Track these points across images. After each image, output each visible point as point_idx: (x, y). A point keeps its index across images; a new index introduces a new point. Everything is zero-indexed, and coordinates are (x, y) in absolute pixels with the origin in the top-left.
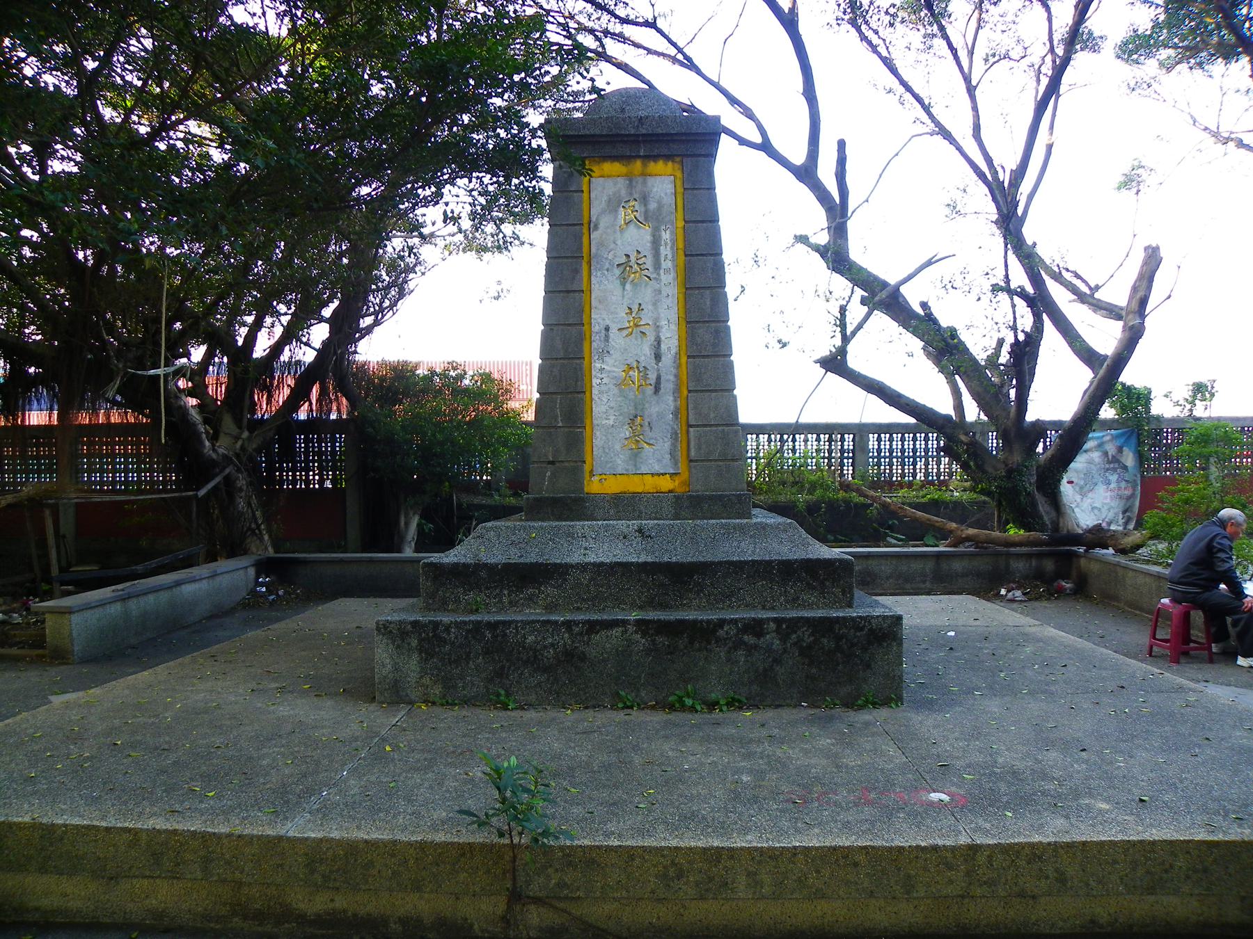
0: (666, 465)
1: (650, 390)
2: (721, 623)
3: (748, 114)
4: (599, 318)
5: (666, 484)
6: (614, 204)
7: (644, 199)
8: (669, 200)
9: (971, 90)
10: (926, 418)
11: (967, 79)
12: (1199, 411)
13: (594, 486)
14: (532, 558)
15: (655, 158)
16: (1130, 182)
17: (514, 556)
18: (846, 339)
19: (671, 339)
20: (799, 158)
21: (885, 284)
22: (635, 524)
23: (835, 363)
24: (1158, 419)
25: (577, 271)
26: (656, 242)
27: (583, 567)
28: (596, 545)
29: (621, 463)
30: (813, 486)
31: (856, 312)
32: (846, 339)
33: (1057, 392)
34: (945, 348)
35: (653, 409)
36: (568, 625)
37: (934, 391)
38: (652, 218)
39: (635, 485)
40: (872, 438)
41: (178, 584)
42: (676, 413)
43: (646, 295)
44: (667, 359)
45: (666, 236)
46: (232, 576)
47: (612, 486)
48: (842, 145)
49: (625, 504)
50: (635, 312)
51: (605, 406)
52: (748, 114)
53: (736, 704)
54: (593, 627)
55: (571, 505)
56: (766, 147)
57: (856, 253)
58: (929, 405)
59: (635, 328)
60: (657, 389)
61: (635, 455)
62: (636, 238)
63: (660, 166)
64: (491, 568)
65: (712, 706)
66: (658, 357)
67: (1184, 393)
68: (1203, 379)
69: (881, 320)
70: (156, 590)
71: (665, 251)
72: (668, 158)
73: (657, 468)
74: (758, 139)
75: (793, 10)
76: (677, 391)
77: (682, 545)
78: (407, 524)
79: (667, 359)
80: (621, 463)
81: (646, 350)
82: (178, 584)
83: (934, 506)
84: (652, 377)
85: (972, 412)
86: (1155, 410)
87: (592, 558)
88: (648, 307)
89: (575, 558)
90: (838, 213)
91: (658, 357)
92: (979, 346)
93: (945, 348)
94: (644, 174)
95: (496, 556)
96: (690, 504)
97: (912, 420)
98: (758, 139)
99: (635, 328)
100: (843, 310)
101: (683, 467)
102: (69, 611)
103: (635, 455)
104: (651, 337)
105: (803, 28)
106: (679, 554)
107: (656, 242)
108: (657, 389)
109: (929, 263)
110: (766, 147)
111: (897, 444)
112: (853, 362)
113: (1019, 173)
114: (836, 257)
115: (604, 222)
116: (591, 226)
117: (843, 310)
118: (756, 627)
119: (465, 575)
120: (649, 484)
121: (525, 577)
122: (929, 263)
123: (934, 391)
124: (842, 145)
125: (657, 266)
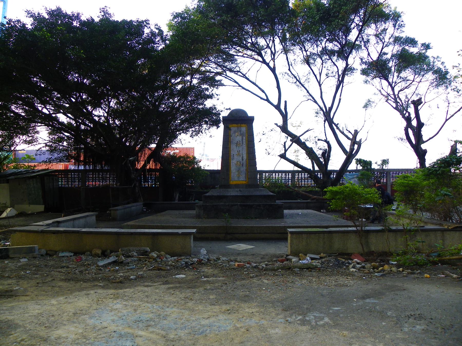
0: (244, 179)
1: (241, 166)
2: (254, 205)
3: (263, 91)
4: (232, 153)
5: (244, 182)
6: (235, 132)
7: (240, 131)
8: (245, 131)
9: (320, 85)
10: (304, 170)
11: (319, 83)
12: (384, 167)
13: (231, 183)
14: (222, 194)
15: (242, 124)
16: (366, 106)
17: (218, 194)
18: (286, 150)
19: (245, 157)
20: (276, 103)
21: (297, 136)
22: (239, 189)
23: (283, 156)
24: (374, 169)
25: (228, 144)
26: (242, 139)
27: (230, 196)
28: (232, 193)
29: (236, 179)
30: (280, 187)
31: (289, 143)
32: (286, 150)
33: (335, 163)
34: (310, 153)
35: (242, 169)
36: (228, 205)
37: (307, 163)
38: (242, 135)
39: (239, 183)
40: (274, 174)
41: (132, 206)
42: (246, 170)
43: (241, 149)
44: (244, 160)
45: (244, 138)
46: (136, 207)
47: (235, 183)
48: (286, 102)
49: (237, 186)
50: (239, 152)
51: (233, 168)
52: (263, 91)
53: (256, 218)
54: (232, 205)
55: (227, 186)
56: (267, 100)
57: (290, 128)
58: (306, 167)
59: (239, 155)
60: (243, 165)
61: (239, 177)
62: (239, 138)
63: (243, 125)
64: (215, 196)
65: (252, 218)
66: (243, 160)
67: (380, 163)
68: (385, 159)
69: (295, 146)
70: (128, 207)
71: (244, 141)
72: (245, 123)
73: (243, 180)
74: (265, 98)
75: (274, 67)
76: (246, 166)
77: (246, 193)
78: (176, 196)
79: (244, 160)
80: (236, 179)
81: (241, 158)
82: (132, 206)
83: (311, 192)
84: (242, 163)
85: (317, 168)
86: (373, 167)
87: (232, 194)
88: (241, 151)
89: (229, 195)
90: (285, 117)
91: (243, 160)
92: (319, 153)
93: (310, 153)
94: (240, 127)
95: (215, 194)
96: (248, 186)
97: (300, 170)
98: (265, 98)
99: (239, 155)
100: (285, 143)
101: (247, 179)
102: (117, 210)
103: (239, 177)
104: (241, 156)
105: (277, 72)
106: (246, 194)
107: (242, 139)
108: (243, 165)
109: (307, 131)
110: (267, 100)
111: (284, 176)
112: (288, 155)
113: (331, 108)
114: (284, 128)
115: (233, 135)
116: (231, 136)
117: (285, 143)
118: (259, 206)
119: (211, 197)
120: (241, 182)
121: (220, 198)
122: (307, 131)
123: (307, 163)
124: (286, 102)
125: (243, 143)
